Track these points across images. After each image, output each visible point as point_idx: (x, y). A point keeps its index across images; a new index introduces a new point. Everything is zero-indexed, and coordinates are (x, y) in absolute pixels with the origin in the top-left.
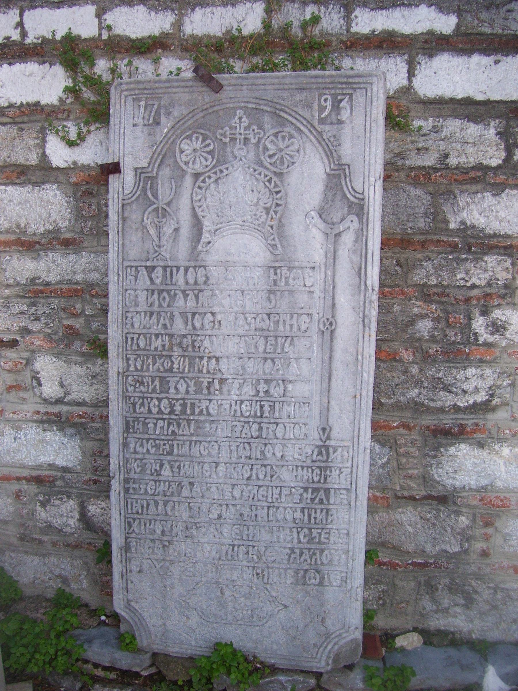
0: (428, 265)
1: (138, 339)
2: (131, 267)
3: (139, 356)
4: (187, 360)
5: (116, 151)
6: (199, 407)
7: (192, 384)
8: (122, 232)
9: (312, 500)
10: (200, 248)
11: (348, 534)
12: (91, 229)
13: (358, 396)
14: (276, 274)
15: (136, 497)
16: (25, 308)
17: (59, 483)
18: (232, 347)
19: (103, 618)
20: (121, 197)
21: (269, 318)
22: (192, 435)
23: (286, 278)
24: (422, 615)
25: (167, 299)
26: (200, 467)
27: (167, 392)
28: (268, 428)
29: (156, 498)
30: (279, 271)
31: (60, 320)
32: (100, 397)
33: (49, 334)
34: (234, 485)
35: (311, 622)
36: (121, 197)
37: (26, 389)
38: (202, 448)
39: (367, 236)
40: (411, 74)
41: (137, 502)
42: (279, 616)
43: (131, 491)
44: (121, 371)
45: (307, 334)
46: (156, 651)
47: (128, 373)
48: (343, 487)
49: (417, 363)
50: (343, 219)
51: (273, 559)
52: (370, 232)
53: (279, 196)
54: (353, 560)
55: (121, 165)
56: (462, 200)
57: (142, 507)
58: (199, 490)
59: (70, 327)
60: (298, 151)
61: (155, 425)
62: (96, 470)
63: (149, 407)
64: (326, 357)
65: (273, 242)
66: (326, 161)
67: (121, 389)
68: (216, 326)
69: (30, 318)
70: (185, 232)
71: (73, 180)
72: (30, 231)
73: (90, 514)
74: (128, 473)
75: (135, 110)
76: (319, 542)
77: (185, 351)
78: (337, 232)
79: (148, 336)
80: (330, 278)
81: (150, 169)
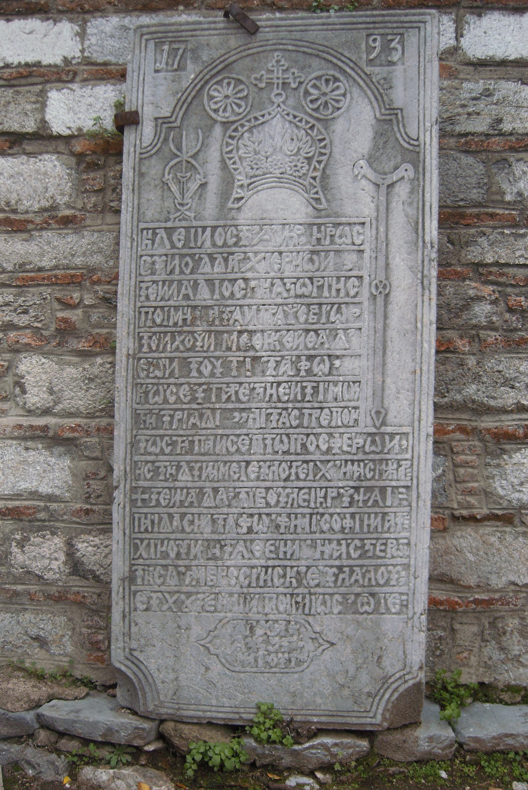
0: (484, 241)
1: (153, 313)
4: (213, 336)
5: (134, 100)
6: (227, 393)
7: (218, 364)
8: (138, 190)
9: (365, 502)
10: (230, 205)
11: (408, 544)
12: (95, 206)
13: (418, 371)
14: (319, 231)
15: (145, 510)
18: (266, 319)
20: (138, 150)
21: (312, 283)
22: (217, 427)
23: (332, 236)
24: (487, 666)
25: (191, 264)
26: (227, 468)
27: (188, 376)
28: (310, 415)
30: (323, 228)
34: (267, 489)
35: (364, 663)
36: (138, 150)
38: (229, 444)
39: (424, 187)
40: (459, 35)
41: (146, 518)
42: (323, 657)
43: (139, 504)
44: (131, 352)
45: (356, 300)
47: (141, 355)
48: (402, 483)
49: (474, 354)
50: (396, 168)
51: (316, 582)
52: (427, 182)
53: (322, 144)
54: (415, 578)
55: (140, 114)
56: (519, 168)
57: (153, 522)
58: (224, 497)
59: (65, 320)
60: (344, 95)
61: (172, 416)
62: (89, 497)
63: (165, 396)
64: (380, 326)
65: (316, 196)
66: (376, 105)
68: (249, 295)
69: (15, 310)
70: (213, 187)
71: (78, 148)
75: (157, 54)
76: (375, 557)
77: (211, 325)
78: (389, 182)
80: (382, 235)
81: (173, 119)
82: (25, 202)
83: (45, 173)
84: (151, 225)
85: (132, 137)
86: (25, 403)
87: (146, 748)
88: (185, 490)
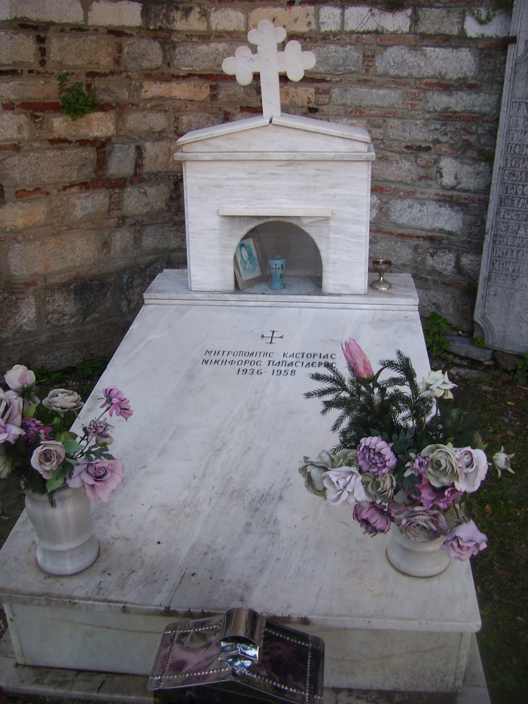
1: (515, 147)
2: (516, 102)
3: (515, 158)
8: (513, 81)
12: (488, 79)
16: (438, 126)
17: (445, 241)
19: (460, 332)
29: (513, 248)
31: (461, 135)
32: (480, 187)
33: (452, 144)
37: (432, 179)
41: (500, 250)
43: (497, 242)
44: (501, 166)
46: (496, 349)
55: (518, 38)
59: (466, 141)
61: (519, 201)
62: (470, 235)
63: (516, 190)
67: (500, 178)
69: (440, 133)
71: (480, 46)
72: (447, 77)
73: (462, 264)
74: (497, 231)
79: (522, 146)
82: (449, 74)
83: (462, 59)
84: (518, 101)
85: (513, 50)
86: (441, 183)
87: (485, 363)
88: (521, 239)
